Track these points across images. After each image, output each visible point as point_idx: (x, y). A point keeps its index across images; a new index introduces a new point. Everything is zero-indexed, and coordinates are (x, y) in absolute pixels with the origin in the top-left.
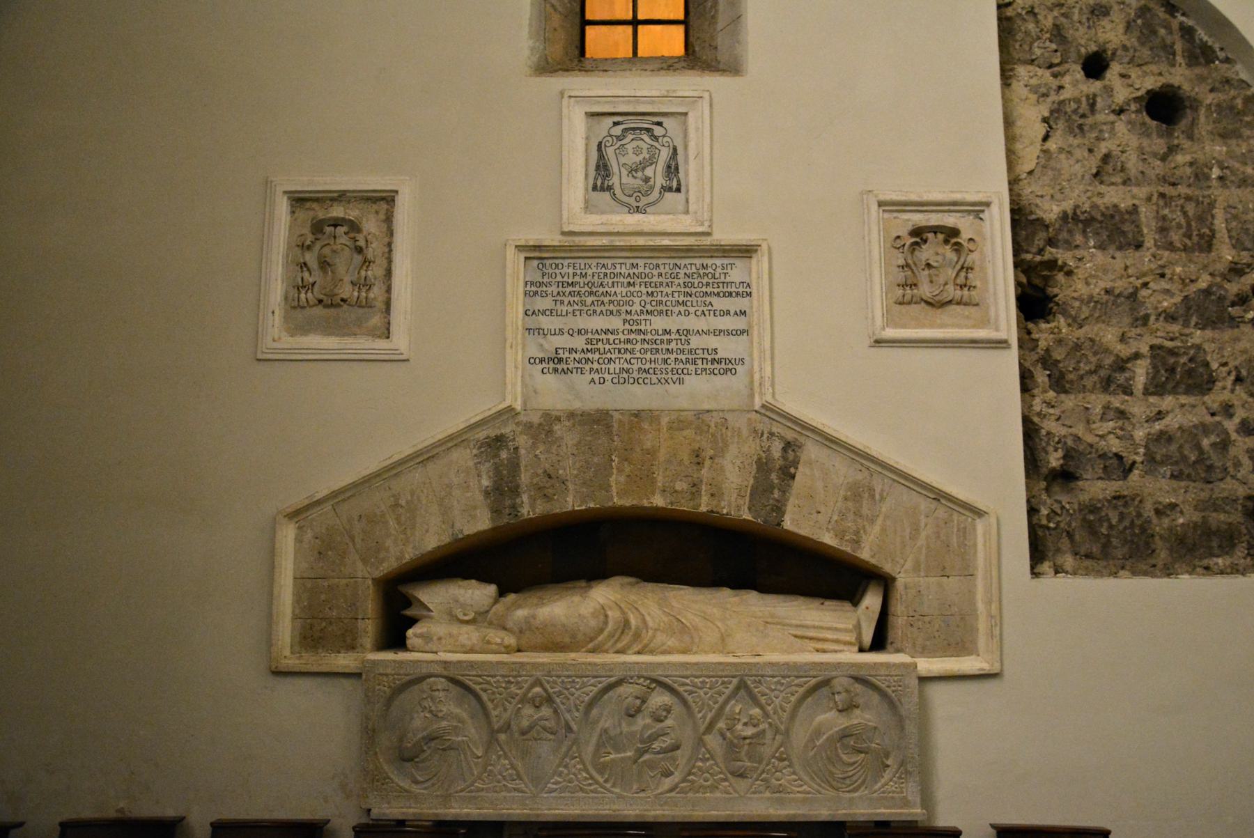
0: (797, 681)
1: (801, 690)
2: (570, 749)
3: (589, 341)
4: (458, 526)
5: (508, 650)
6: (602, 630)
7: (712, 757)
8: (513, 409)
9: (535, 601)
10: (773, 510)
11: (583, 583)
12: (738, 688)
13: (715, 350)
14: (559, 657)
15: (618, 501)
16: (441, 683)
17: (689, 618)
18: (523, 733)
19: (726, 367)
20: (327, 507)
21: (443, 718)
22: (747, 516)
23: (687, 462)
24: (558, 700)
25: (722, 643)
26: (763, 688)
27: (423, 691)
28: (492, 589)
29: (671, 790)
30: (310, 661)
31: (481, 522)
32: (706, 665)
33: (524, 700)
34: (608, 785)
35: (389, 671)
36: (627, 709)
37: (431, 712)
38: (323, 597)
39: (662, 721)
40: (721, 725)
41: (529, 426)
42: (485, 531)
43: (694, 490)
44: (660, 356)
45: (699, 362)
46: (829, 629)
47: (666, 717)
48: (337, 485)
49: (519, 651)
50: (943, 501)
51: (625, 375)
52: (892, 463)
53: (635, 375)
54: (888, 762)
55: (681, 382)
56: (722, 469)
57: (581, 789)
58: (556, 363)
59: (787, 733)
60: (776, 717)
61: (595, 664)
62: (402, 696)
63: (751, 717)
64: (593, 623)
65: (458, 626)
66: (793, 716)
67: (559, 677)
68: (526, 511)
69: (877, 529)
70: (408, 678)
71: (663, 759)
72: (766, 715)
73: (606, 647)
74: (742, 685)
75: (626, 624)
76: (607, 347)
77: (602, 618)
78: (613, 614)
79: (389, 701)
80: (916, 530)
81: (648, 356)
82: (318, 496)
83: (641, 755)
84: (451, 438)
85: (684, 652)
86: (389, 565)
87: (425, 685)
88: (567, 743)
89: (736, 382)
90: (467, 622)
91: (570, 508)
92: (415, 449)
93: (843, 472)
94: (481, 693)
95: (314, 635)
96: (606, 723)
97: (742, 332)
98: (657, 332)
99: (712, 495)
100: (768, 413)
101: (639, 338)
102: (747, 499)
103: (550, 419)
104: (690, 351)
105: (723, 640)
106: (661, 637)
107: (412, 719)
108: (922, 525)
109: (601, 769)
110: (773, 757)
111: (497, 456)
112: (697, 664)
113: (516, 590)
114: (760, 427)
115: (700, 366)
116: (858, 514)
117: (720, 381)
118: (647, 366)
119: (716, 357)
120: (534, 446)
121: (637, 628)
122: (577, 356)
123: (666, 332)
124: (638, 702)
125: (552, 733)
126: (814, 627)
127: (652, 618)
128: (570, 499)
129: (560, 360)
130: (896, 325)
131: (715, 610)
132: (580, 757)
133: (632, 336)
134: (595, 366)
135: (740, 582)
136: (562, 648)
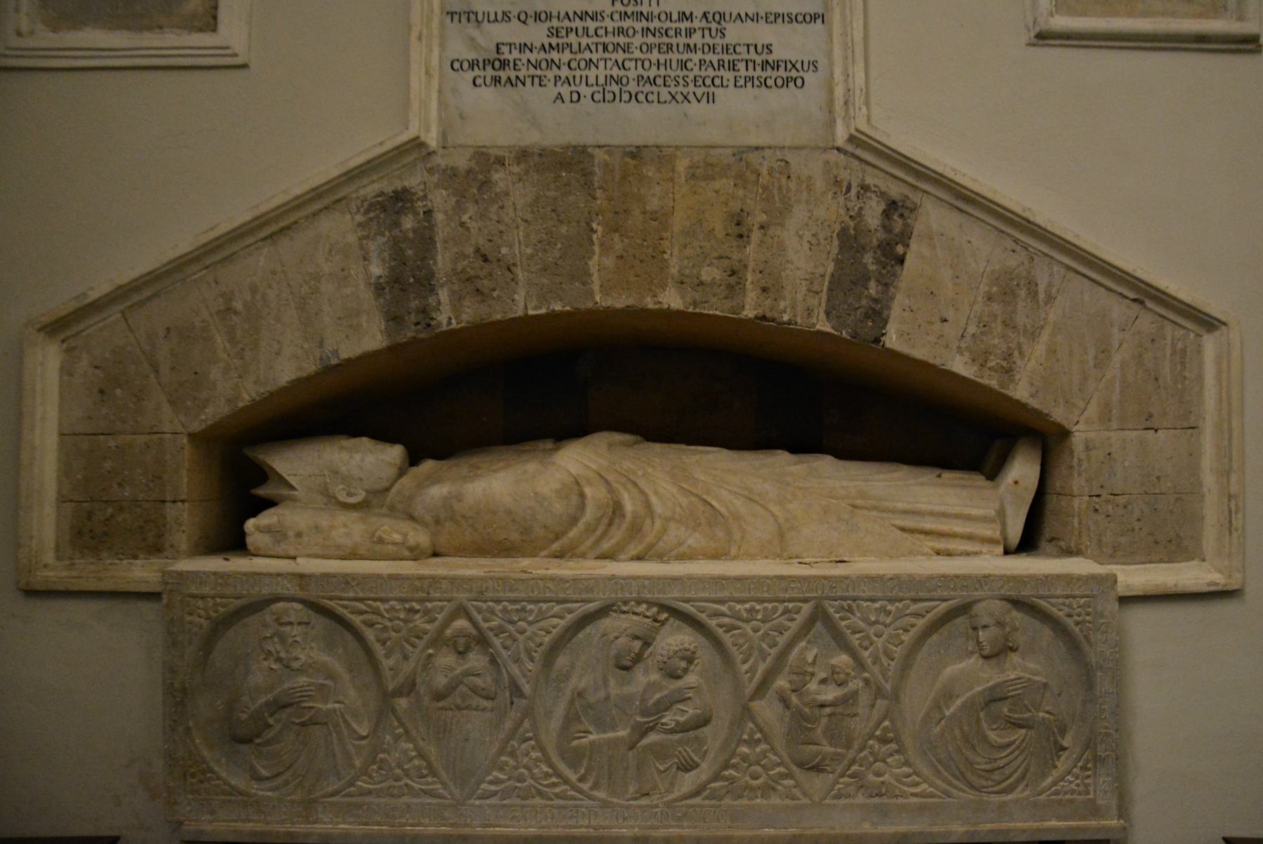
0: (914, 607)
1: (921, 623)
2: (518, 725)
3: (555, 32)
4: (329, 346)
5: (416, 554)
6: (574, 520)
7: (766, 739)
8: (422, 145)
10: (867, 316)
11: (549, 444)
13: (768, 47)
15: (601, 300)
18: (439, 696)
19: (789, 75)
20: (114, 314)
21: (300, 671)
22: (824, 326)
23: (720, 234)
24: (497, 642)
25: (780, 545)
26: (856, 620)
27: (265, 625)
28: (395, 453)
29: (696, 793)
30: (86, 573)
31: (371, 337)
32: (759, 581)
33: (438, 641)
34: (585, 787)
35: (206, 590)
36: (618, 657)
37: (279, 660)
38: (108, 465)
39: (679, 677)
40: (782, 683)
41: (451, 174)
43: (732, 280)
44: (674, 56)
45: (741, 66)
46: (957, 516)
47: (686, 671)
48: (127, 275)
49: (435, 555)
50: (1149, 304)
51: (615, 88)
52: (1069, 237)
53: (633, 87)
54: (1065, 744)
55: (711, 98)
56: (782, 248)
57: (540, 793)
58: (497, 68)
59: (895, 697)
61: (562, 580)
63: (834, 670)
64: (559, 507)
65: (340, 516)
66: (906, 666)
67: (498, 601)
68: (445, 318)
69: (1040, 349)
70: (238, 603)
71: (680, 742)
72: (860, 664)
73: (583, 548)
74: (819, 615)
75: (617, 508)
76: (584, 41)
77: (575, 499)
79: (208, 645)
80: (1104, 352)
81: (654, 56)
82: (94, 295)
83: (644, 734)
84: (317, 193)
85: (716, 556)
86: (215, 412)
88: (513, 715)
89: (807, 99)
91: (520, 313)
92: (257, 213)
93: (985, 251)
95: (91, 532)
97: (814, 18)
98: (669, 17)
99: (764, 290)
100: (859, 152)
101: (638, 26)
102: (824, 296)
103: (486, 160)
104: (726, 49)
105: (782, 536)
106: (675, 533)
108: (1115, 344)
110: (871, 736)
111: (397, 224)
112: (739, 579)
113: (441, 455)
114: (844, 175)
115: (743, 72)
116: (1009, 324)
117: (776, 98)
118: (653, 72)
119: (770, 58)
120: (459, 208)
121: (635, 516)
122: (533, 57)
123: (684, 16)
124: (637, 645)
125: (487, 698)
126: (932, 514)
128: (520, 297)
129: (504, 64)
130: (1071, 12)
132: (536, 738)
133: (626, 24)
134: (565, 72)
135: (802, 443)
136: (507, 550)
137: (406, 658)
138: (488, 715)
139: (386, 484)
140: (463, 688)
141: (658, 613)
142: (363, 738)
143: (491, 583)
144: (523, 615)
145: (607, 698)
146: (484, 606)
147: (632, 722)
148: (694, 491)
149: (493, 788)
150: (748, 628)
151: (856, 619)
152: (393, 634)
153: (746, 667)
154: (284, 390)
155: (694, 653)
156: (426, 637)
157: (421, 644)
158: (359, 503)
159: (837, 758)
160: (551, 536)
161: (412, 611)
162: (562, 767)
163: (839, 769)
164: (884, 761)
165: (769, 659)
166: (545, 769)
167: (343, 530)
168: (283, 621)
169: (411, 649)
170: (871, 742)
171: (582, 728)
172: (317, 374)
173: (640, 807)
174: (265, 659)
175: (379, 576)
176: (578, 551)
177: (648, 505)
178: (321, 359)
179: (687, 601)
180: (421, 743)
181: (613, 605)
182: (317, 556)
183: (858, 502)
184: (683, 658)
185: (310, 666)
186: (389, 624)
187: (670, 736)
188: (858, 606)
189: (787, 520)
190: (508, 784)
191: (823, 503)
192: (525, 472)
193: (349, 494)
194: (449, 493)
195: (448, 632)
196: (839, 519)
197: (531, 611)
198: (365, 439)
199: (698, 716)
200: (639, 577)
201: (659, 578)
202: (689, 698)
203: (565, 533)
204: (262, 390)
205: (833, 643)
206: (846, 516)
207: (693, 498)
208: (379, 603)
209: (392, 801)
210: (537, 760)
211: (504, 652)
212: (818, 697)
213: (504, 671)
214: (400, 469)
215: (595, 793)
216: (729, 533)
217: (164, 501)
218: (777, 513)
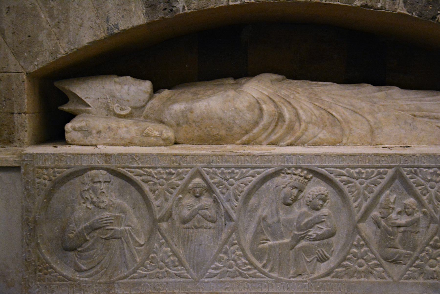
2: (229, 236)
4: (113, 21)
5: (167, 143)
6: (256, 123)
7: (367, 244)
9: (190, 96)
11: (232, 81)
12: (393, 179)
14: (217, 149)
16: (103, 175)
17: (340, 112)
18: (184, 221)
22: (402, 10)
24: (218, 190)
25: (372, 136)
26: (419, 179)
27: (84, 184)
28: (147, 85)
29: (327, 275)
32: (364, 156)
33: (184, 190)
34: (266, 270)
35: (48, 164)
36: (285, 198)
37: (93, 203)
39: (318, 210)
40: (375, 213)
42: (140, 26)
47: (322, 206)
49: (176, 143)
57: (241, 275)
60: (430, 207)
62: (63, 188)
64: (248, 116)
65: (115, 120)
71: (319, 245)
72: (421, 203)
73: (260, 139)
74: (398, 175)
75: (281, 116)
77: (257, 111)
78: (267, 108)
83: (298, 241)
85: (334, 144)
86: (42, 61)
87: (86, 178)
88: (226, 231)
90: (124, 117)
91: (225, 4)
94: (143, 184)
96: (264, 211)
106: (312, 130)
107: (73, 210)
109: (260, 254)
110: (428, 244)
121: (291, 121)
124: (295, 191)
125: (212, 222)
127: (304, 111)
131: (364, 104)
132: (239, 243)
135: (379, 80)
137: (166, 200)
138: (212, 231)
139: (143, 103)
140: (198, 216)
141: (307, 174)
142: (141, 246)
143: (215, 158)
144: (233, 175)
145: (279, 221)
146: (211, 171)
147: (292, 234)
148: (323, 107)
149: (215, 272)
150: (357, 182)
151: (419, 178)
152: (159, 187)
153: (356, 204)
154: (85, 48)
155: (326, 196)
156: (178, 188)
157: (175, 192)
158: (127, 114)
159: (408, 256)
160: (243, 132)
161: (171, 174)
162: (253, 259)
163: (409, 262)
164: (435, 259)
165: (369, 200)
166: (244, 261)
167: (125, 129)
168: (96, 180)
169: (169, 195)
170: (427, 248)
171: (265, 238)
172: (105, 38)
173: (296, 282)
174: (84, 203)
175: (152, 155)
176: (257, 141)
177: (297, 115)
178: (108, 30)
179: (323, 167)
180: (175, 247)
181: (282, 170)
182: (109, 145)
183: (417, 113)
184: (321, 199)
185: (111, 206)
186: (157, 181)
187: (313, 242)
188: (420, 171)
189: (375, 123)
190: (223, 269)
191: (397, 114)
192: (228, 96)
193: (122, 109)
194: (185, 108)
195: (190, 185)
196: (406, 123)
197: (237, 173)
198: (129, 77)
199: (328, 231)
200: (297, 154)
201: (308, 155)
202: (324, 221)
203: (251, 130)
204: (72, 48)
205: (405, 192)
206: (410, 121)
207: (322, 111)
208: (151, 170)
209: (158, 280)
210: (240, 255)
211: (222, 196)
212: (397, 221)
213: (222, 206)
214: (150, 95)
215: (272, 274)
216: (342, 130)
217: (13, 113)
218: (370, 119)
